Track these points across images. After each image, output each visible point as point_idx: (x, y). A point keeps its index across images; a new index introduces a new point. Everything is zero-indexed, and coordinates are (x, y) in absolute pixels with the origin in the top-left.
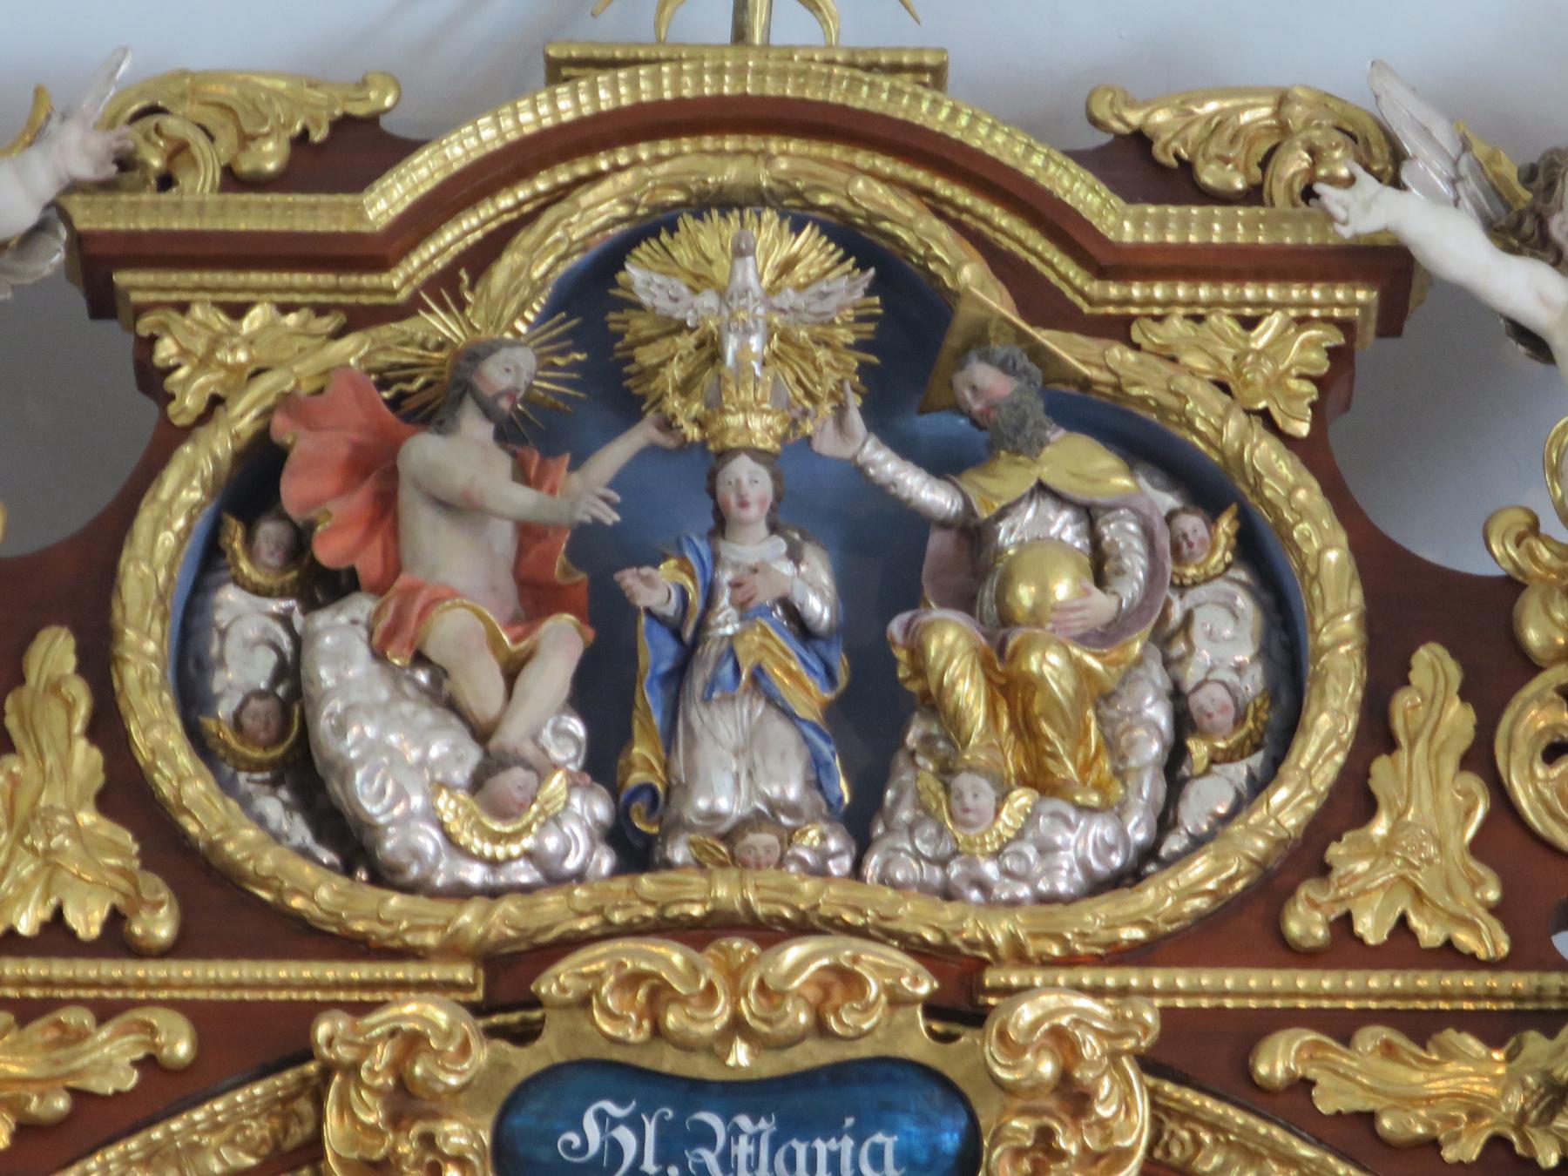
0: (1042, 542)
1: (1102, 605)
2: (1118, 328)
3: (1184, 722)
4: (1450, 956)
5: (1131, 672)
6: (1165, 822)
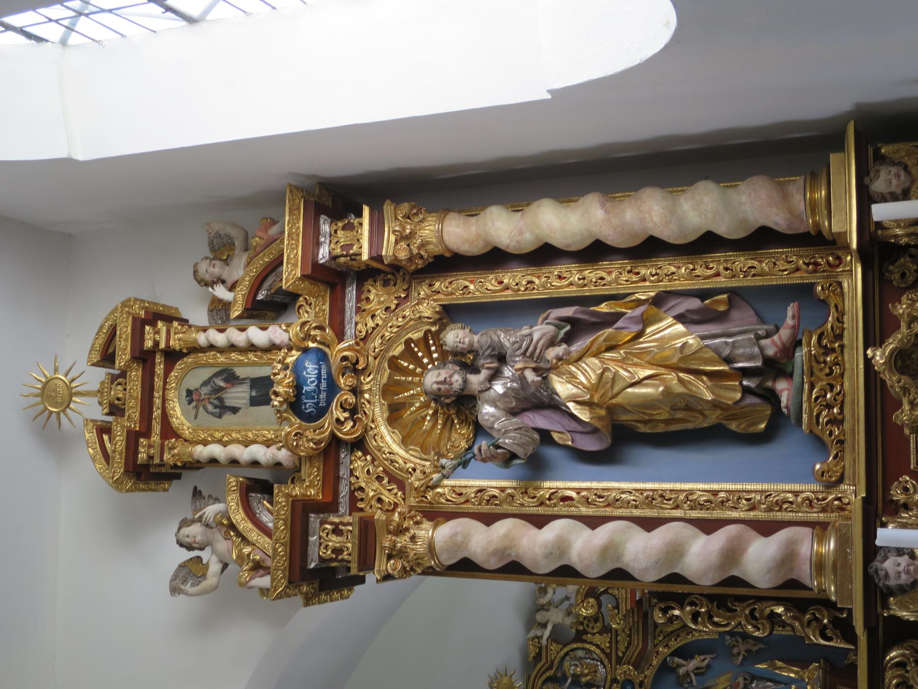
0: (574, 670)
1: (580, 666)
2: (552, 662)
3: (589, 658)
4: (611, 638)
5: (585, 663)
6: (597, 660)
